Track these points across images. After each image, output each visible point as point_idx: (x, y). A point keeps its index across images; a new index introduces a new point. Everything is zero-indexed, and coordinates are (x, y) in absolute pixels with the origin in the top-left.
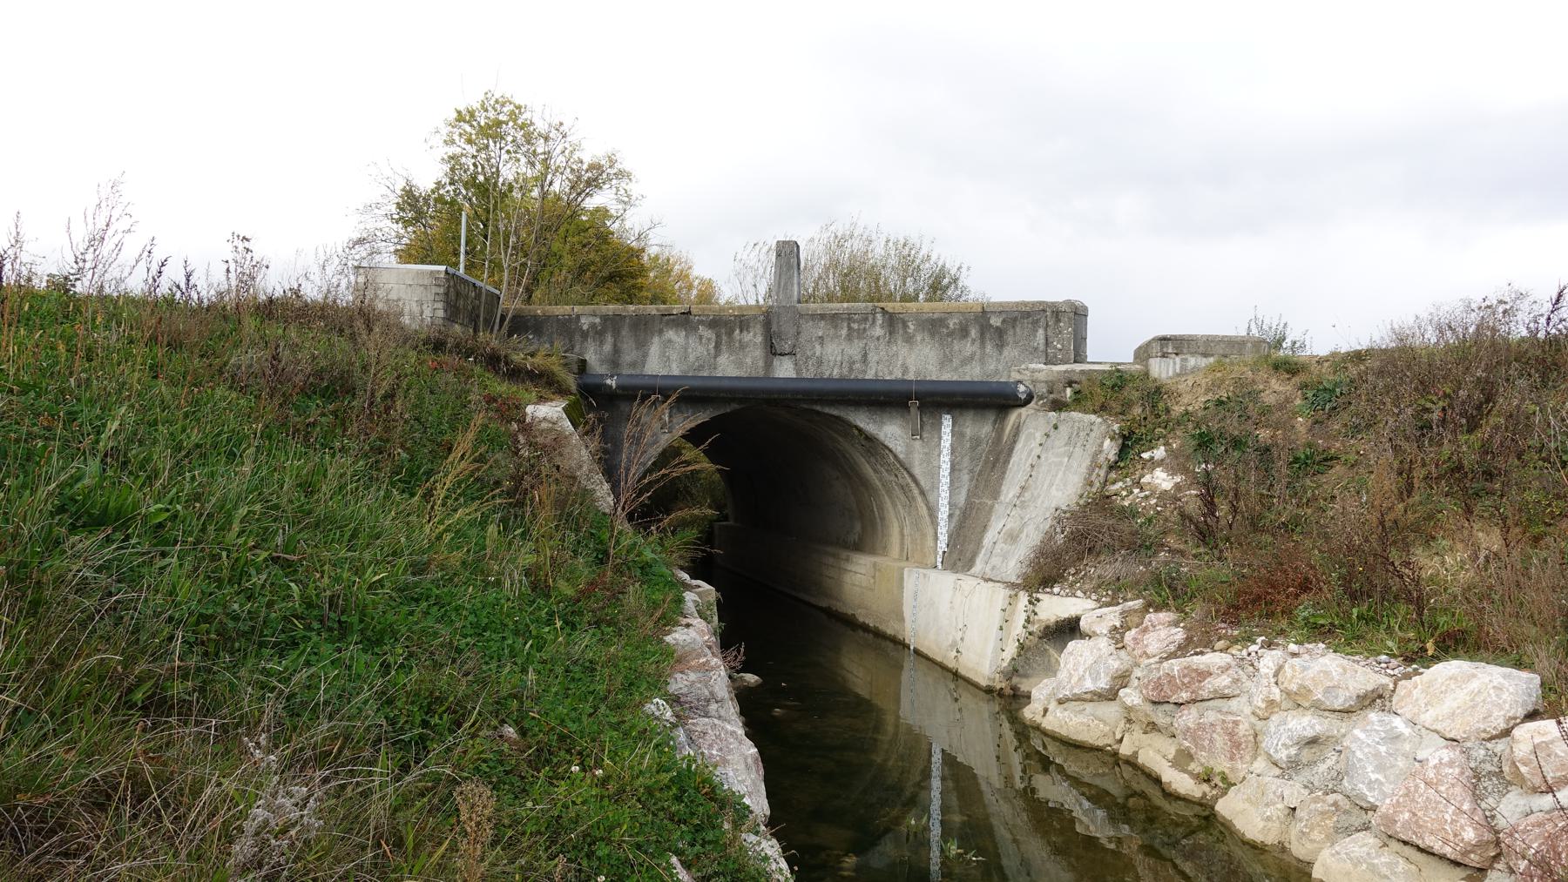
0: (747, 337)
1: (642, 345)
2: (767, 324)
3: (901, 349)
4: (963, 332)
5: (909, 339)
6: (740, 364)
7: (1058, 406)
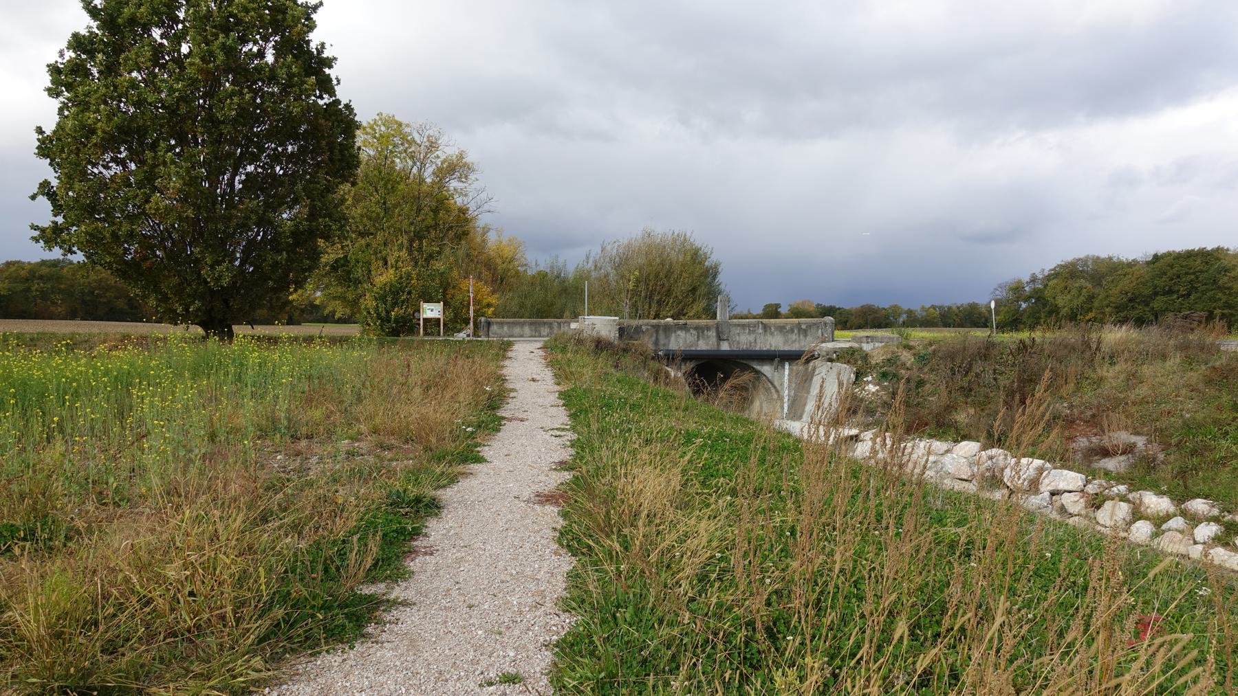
0: (710, 333)
1: (667, 337)
2: (717, 328)
3: (769, 338)
5: (772, 334)
6: (707, 344)
7: (831, 360)
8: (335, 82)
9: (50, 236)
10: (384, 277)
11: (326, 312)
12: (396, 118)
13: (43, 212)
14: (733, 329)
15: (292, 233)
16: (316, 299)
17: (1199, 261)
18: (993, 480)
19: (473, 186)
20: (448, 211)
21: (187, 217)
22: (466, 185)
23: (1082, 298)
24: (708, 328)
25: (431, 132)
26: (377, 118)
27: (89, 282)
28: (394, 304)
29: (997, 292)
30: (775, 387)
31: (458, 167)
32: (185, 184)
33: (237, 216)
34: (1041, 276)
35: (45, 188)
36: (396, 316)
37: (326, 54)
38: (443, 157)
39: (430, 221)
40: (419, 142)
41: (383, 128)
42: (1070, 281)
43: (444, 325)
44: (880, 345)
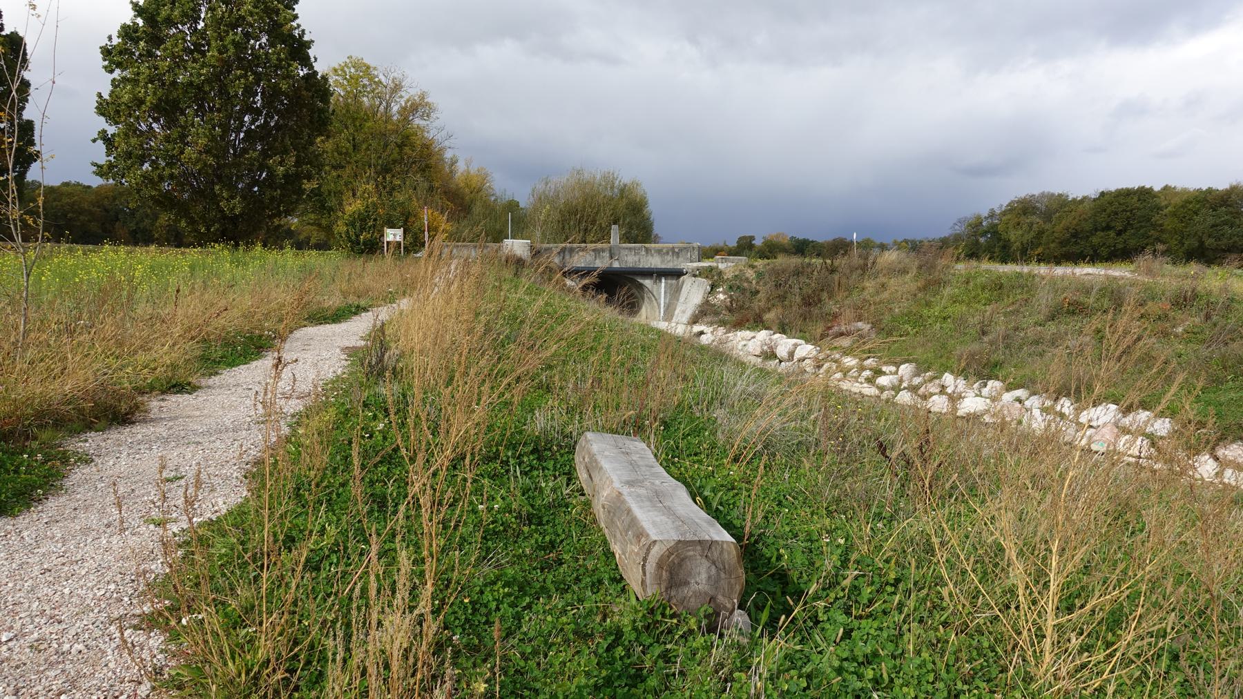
0: (604, 254)
2: (610, 251)
3: (650, 258)
4: (668, 253)
5: (652, 255)
7: (695, 276)
8: (313, 60)
9: (101, 171)
10: (353, 207)
11: (301, 237)
12: (364, 61)
13: (100, 154)
14: (622, 251)
15: (284, 175)
16: (292, 224)
17: (1136, 199)
18: (770, 355)
19: (435, 124)
20: (413, 147)
21: (210, 164)
22: (428, 122)
23: (1032, 234)
24: (603, 251)
25: (395, 75)
26: (348, 61)
27: (62, 205)
28: (362, 229)
29: (957, 227)
30: (654, 296)
31: (418, 107)
32: (209, 141)
33: (245, 164)
34: (999, 212)
35: (103, 135)
36: (364, 239)
37: (306, 38)
38: (407, 97)
39: (396, 156)
40: (385, 84)
41: (353, 70)
42: (1023, 217)
43: (404, 248)
44: (732, 264)
